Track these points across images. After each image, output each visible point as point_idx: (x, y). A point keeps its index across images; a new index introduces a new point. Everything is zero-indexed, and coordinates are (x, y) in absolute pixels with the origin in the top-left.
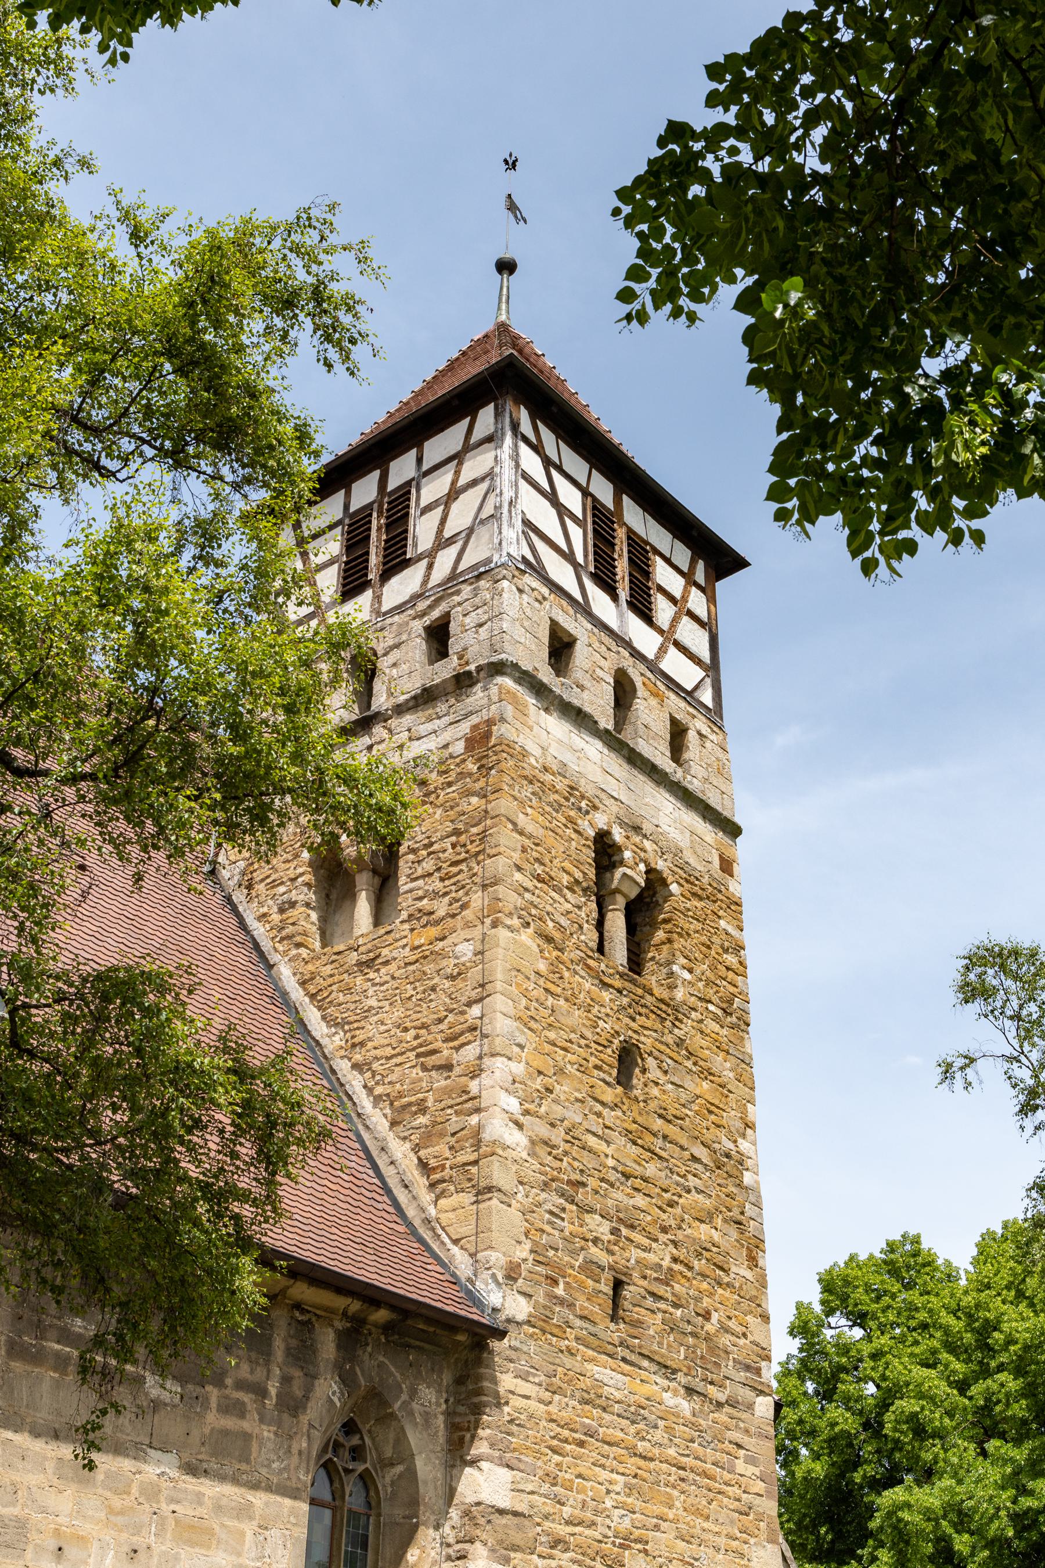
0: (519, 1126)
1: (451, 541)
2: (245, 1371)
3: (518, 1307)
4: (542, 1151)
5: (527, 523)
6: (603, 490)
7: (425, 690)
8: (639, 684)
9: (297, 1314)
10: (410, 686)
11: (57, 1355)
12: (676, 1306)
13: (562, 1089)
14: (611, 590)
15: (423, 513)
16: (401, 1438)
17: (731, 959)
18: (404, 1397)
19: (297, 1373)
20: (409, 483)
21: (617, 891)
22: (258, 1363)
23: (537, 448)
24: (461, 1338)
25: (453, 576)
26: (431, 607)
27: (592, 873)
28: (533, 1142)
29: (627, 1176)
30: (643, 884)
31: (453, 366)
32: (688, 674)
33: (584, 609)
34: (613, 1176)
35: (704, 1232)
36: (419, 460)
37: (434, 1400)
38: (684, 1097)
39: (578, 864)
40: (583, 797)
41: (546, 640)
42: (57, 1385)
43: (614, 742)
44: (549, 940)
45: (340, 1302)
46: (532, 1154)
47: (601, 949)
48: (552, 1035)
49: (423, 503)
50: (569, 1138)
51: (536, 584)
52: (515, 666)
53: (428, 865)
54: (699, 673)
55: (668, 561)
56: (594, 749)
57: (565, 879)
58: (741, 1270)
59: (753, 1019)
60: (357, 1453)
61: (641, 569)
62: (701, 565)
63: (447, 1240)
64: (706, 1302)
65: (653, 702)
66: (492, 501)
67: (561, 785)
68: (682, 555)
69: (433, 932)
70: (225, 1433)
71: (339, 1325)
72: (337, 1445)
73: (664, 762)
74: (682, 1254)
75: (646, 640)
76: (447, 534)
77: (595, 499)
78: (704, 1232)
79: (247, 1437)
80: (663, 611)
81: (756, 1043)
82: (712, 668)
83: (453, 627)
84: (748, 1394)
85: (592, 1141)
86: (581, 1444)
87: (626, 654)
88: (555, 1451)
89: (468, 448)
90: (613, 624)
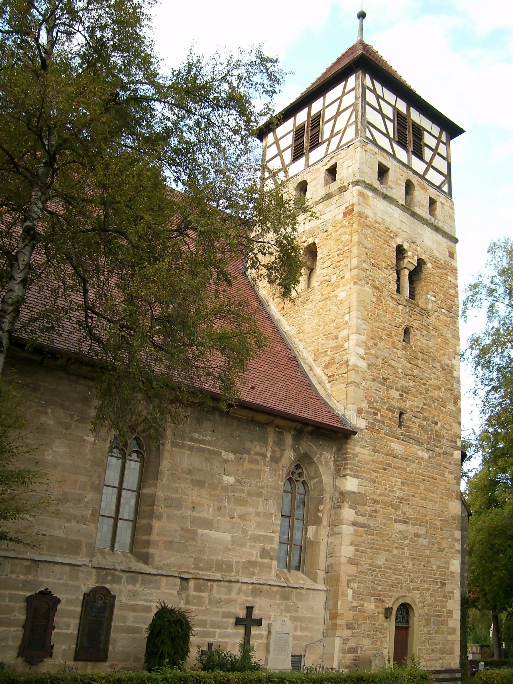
1: (337, 133)
2: (258, 449)
6: (402, 106)
9: (277, 429)
11: (189, 445)
14: (404, 146)
16: (317, 470)
18: (318, 456)
19: (277, 449)
21: (406, 268)
22: (263, 446)
27: (395, 262)
29: (406, 375)
37: (329, 457)
40: (391, 232)
49: (326, 120)
50: (383, 362)
52: (363, 182)
53: (328, 263)
55: (430, 133)
56: (397, 212)
57: (384, 265)
62: (444, 134)
63: (335, 401)
65: (422, 191)
68: (436, 130)
69: (331, 288)
70: (251, 470)
72: (293, 473)
76: (335, 131)
79: (259, 471)
80: (428, 154)
82: (448, 177)
86: (385, 469)
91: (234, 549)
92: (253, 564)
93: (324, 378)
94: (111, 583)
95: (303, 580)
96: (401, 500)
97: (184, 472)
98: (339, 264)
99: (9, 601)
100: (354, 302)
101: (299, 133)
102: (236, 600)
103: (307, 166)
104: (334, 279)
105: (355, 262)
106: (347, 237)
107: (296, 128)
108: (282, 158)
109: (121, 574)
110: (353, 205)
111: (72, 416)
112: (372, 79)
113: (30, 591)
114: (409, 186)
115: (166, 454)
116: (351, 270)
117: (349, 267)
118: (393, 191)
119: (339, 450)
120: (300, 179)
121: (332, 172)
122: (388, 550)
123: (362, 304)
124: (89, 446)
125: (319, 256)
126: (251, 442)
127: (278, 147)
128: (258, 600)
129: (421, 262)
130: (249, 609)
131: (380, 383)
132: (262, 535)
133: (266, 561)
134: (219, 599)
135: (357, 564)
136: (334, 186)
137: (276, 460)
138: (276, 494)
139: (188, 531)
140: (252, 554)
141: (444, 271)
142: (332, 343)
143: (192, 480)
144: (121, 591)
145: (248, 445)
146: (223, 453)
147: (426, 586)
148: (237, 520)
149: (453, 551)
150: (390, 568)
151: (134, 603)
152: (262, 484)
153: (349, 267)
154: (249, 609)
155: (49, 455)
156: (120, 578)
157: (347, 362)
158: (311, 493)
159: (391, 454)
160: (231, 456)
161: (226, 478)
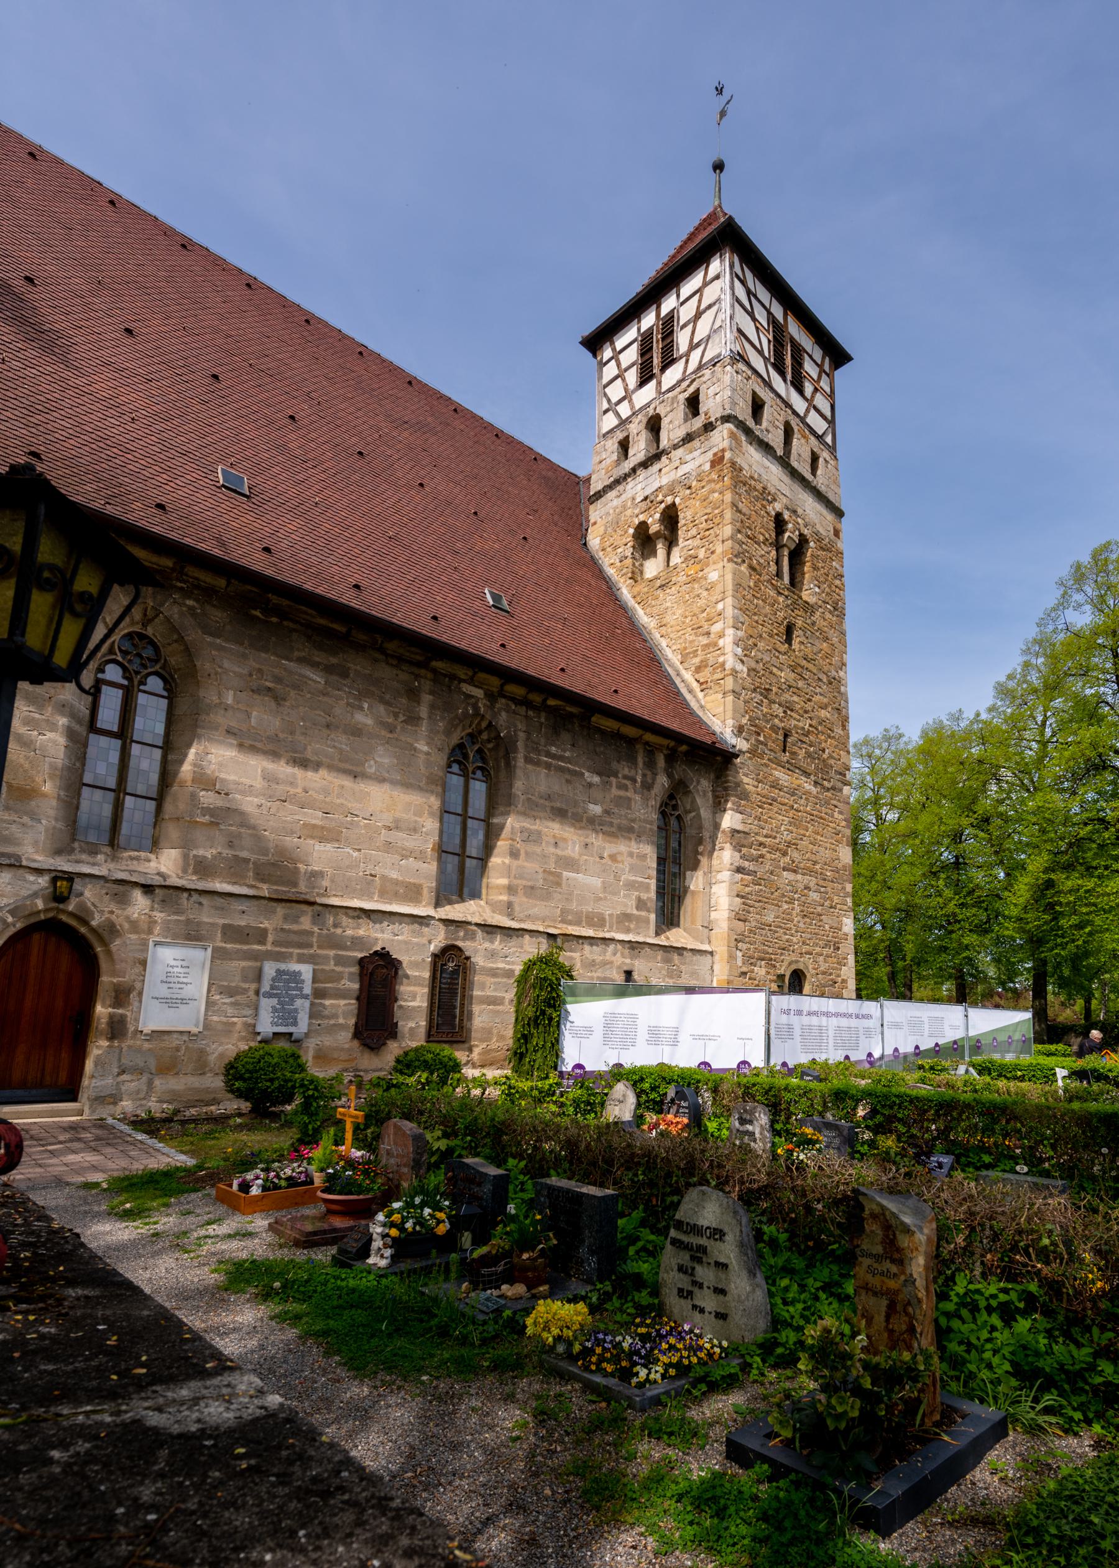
0: (742, 662)
1: (698, 345)
2: (626, 771)
3: (742, 744)
4: (752, 674)
5: (739, 331)
6: (778, 311)
7: (688, 434)
8: (796, 431)
10: (681, 433)
11: (546, 762)
12: (811, 746)
13: (761, 645)
14: (782, 373)
15: (682, 328)
16: (694, 801)
17: (837, 582)
19: (649, 773)
20: (673, 311)
21: (785, 545)
23: (743, 282)
24: (719, 758)
25: (700, 367)
26: (689, 386)
27: (773, 535)
28: (749, 670)
29: (790, 687)
30: (245, 1106)
31: (690, 239)
32: (820, 426)
33: (768, 384)
34: (784, 687)
35: (823, 713)
36: (678, 296)
38: (815, 649)
39: (767, 530)
41: (750, 403)
42: (547, 776)
43: (784, 462)
44: (754, 569)
45: (665, 742)
46: (748, 675)
47: (777, 575)
48: (756, 618)
49: (681, 323)
51: (745, 368)
52: (736, 417)
53: (694, 532)
54: (825, 425)
55: (810, 357)
57: (761, 538)
58: (839, 731)
59: (847, 612)
60: (675, 807)
61: (798, 364)
62: (827, 360)
64: (823, 745)
65: (803, 441)
66: (721, 316)
67: (759, 487)
68: (818, 354)
69: (698, 567)
70: (621, 797)
71: (665, 752)
72: (667, 804)
73: (808, 476)
74: (814, 723)
75: (800, 405)
76: (696, 341)
77: (774, 317)
78: (823, 713)
79: (629, 799)
80: (808, 389)
81: (849, 624)
82: (831, 422)
83: (702, 397)
84: (839, 785)
85: (775, 670)
86: (771, 804)
87: (790, 412)
88: (760, 807)
89: (705, 284)
90: (783, 394)
91: (606, 898)
92: (627, 917)
93: (695, 685)
94: (464, 939)
95: (685, 938)
96: (789, 844)
97: (541, 797)
98: (707, 533)
99: (335, 965)
100: (730, 586)
101: (646, 343)
102: (612, 962)
103: (659, 392)
104: (702, 554)
105: (728, 530)
106: (716, 495)
107: (642, 335)
108: (624, 380)
109: (475, 928)
110: (723, 450)
111: (396, 715)
112: (741, 262)
113: (361, 951)
114: (788, 432)
115: (519, 773)
116: (723, 541)
117: (720, 538)
118: (770, 436)
119: (718, 777)
120: (651, 411)
121: (693, 404)
122: (777, 905)
123: (738, 586)
124: (422, 757)
125: (681, 522)
126: (618, 762)
127: (619, 365)
128: (637, 963)
129: (803, 541)
130: (629, 974)
131: (761, 694)
132: (637, 882)
133: (643, 913)
134: (593, 961)
135: (745, 921)
136: (698, 423)
137: (647, 786)
138: (651, 830)
139: (550, 873)
140: (626, 905)
141: (830, 555)
142: (704, 640)
143: (552, 807)
144: (476, 951)
145: (615, 765)
146: (587, 774)
147: (818, 949)
148: (607, 861)
149: (845, 908)
150: (780, 927)
151: (494, 966)
152: (634, 816)
153: (720, 538)
154: (629, 974)
155: (371, 767)
156: (474, 933)
157: (723, 664)
158: (688, 830)
159: (775, 785)
160: (596, 779)
161: (591, 806)
